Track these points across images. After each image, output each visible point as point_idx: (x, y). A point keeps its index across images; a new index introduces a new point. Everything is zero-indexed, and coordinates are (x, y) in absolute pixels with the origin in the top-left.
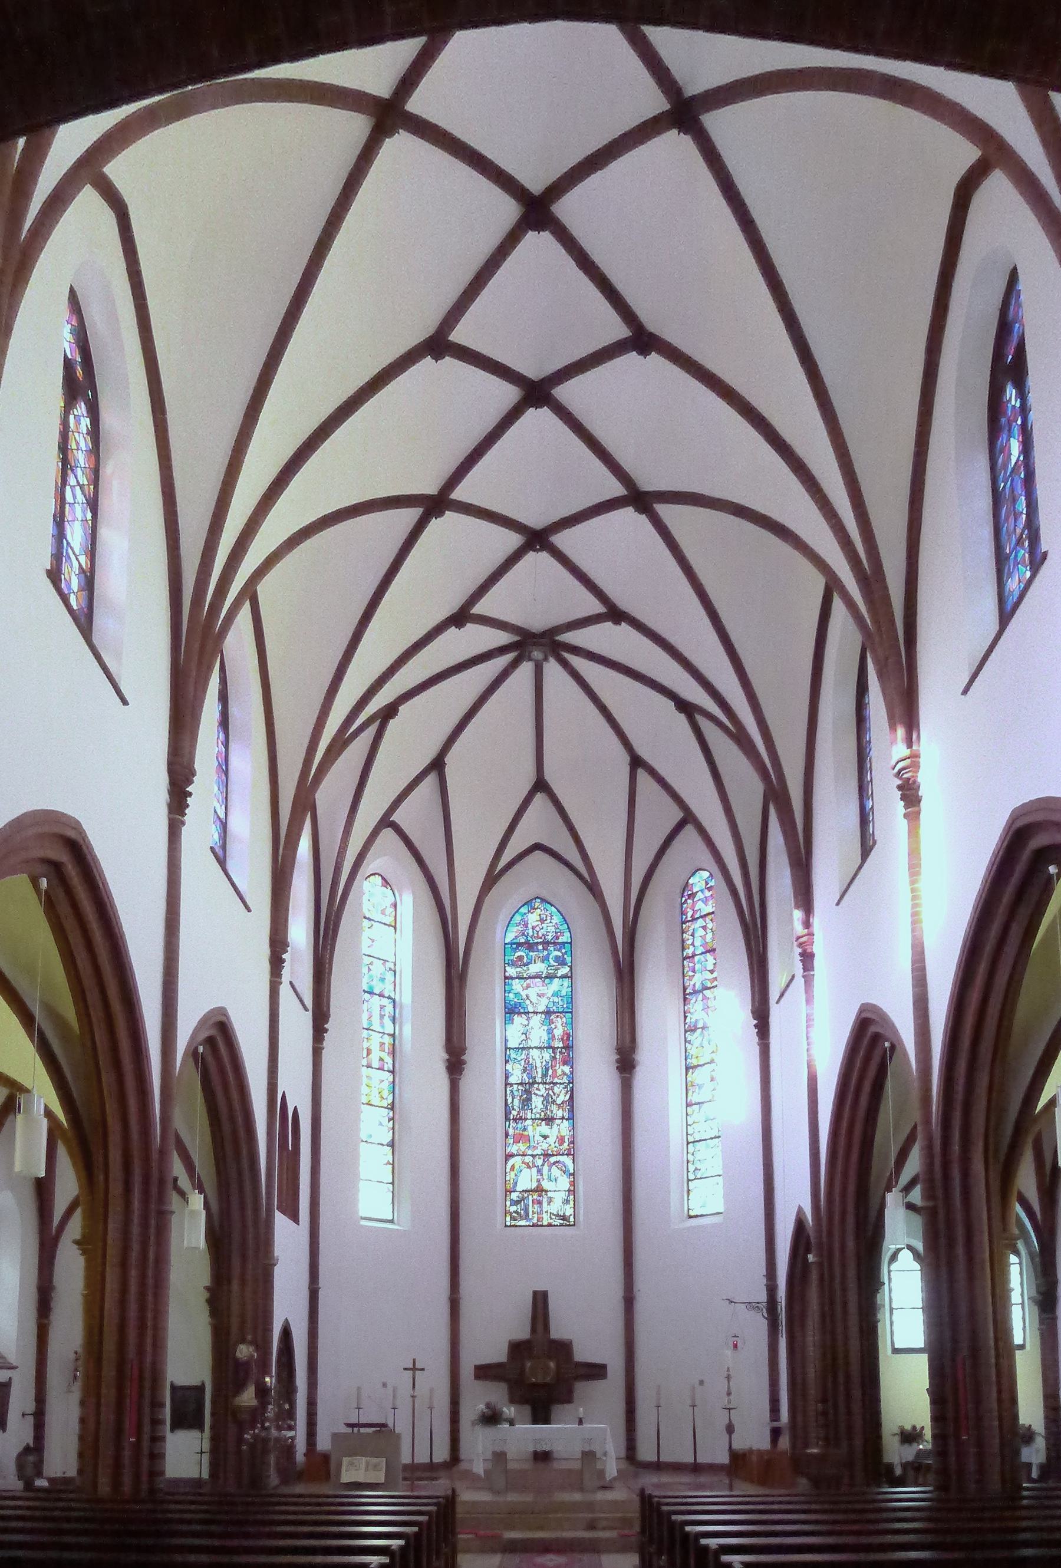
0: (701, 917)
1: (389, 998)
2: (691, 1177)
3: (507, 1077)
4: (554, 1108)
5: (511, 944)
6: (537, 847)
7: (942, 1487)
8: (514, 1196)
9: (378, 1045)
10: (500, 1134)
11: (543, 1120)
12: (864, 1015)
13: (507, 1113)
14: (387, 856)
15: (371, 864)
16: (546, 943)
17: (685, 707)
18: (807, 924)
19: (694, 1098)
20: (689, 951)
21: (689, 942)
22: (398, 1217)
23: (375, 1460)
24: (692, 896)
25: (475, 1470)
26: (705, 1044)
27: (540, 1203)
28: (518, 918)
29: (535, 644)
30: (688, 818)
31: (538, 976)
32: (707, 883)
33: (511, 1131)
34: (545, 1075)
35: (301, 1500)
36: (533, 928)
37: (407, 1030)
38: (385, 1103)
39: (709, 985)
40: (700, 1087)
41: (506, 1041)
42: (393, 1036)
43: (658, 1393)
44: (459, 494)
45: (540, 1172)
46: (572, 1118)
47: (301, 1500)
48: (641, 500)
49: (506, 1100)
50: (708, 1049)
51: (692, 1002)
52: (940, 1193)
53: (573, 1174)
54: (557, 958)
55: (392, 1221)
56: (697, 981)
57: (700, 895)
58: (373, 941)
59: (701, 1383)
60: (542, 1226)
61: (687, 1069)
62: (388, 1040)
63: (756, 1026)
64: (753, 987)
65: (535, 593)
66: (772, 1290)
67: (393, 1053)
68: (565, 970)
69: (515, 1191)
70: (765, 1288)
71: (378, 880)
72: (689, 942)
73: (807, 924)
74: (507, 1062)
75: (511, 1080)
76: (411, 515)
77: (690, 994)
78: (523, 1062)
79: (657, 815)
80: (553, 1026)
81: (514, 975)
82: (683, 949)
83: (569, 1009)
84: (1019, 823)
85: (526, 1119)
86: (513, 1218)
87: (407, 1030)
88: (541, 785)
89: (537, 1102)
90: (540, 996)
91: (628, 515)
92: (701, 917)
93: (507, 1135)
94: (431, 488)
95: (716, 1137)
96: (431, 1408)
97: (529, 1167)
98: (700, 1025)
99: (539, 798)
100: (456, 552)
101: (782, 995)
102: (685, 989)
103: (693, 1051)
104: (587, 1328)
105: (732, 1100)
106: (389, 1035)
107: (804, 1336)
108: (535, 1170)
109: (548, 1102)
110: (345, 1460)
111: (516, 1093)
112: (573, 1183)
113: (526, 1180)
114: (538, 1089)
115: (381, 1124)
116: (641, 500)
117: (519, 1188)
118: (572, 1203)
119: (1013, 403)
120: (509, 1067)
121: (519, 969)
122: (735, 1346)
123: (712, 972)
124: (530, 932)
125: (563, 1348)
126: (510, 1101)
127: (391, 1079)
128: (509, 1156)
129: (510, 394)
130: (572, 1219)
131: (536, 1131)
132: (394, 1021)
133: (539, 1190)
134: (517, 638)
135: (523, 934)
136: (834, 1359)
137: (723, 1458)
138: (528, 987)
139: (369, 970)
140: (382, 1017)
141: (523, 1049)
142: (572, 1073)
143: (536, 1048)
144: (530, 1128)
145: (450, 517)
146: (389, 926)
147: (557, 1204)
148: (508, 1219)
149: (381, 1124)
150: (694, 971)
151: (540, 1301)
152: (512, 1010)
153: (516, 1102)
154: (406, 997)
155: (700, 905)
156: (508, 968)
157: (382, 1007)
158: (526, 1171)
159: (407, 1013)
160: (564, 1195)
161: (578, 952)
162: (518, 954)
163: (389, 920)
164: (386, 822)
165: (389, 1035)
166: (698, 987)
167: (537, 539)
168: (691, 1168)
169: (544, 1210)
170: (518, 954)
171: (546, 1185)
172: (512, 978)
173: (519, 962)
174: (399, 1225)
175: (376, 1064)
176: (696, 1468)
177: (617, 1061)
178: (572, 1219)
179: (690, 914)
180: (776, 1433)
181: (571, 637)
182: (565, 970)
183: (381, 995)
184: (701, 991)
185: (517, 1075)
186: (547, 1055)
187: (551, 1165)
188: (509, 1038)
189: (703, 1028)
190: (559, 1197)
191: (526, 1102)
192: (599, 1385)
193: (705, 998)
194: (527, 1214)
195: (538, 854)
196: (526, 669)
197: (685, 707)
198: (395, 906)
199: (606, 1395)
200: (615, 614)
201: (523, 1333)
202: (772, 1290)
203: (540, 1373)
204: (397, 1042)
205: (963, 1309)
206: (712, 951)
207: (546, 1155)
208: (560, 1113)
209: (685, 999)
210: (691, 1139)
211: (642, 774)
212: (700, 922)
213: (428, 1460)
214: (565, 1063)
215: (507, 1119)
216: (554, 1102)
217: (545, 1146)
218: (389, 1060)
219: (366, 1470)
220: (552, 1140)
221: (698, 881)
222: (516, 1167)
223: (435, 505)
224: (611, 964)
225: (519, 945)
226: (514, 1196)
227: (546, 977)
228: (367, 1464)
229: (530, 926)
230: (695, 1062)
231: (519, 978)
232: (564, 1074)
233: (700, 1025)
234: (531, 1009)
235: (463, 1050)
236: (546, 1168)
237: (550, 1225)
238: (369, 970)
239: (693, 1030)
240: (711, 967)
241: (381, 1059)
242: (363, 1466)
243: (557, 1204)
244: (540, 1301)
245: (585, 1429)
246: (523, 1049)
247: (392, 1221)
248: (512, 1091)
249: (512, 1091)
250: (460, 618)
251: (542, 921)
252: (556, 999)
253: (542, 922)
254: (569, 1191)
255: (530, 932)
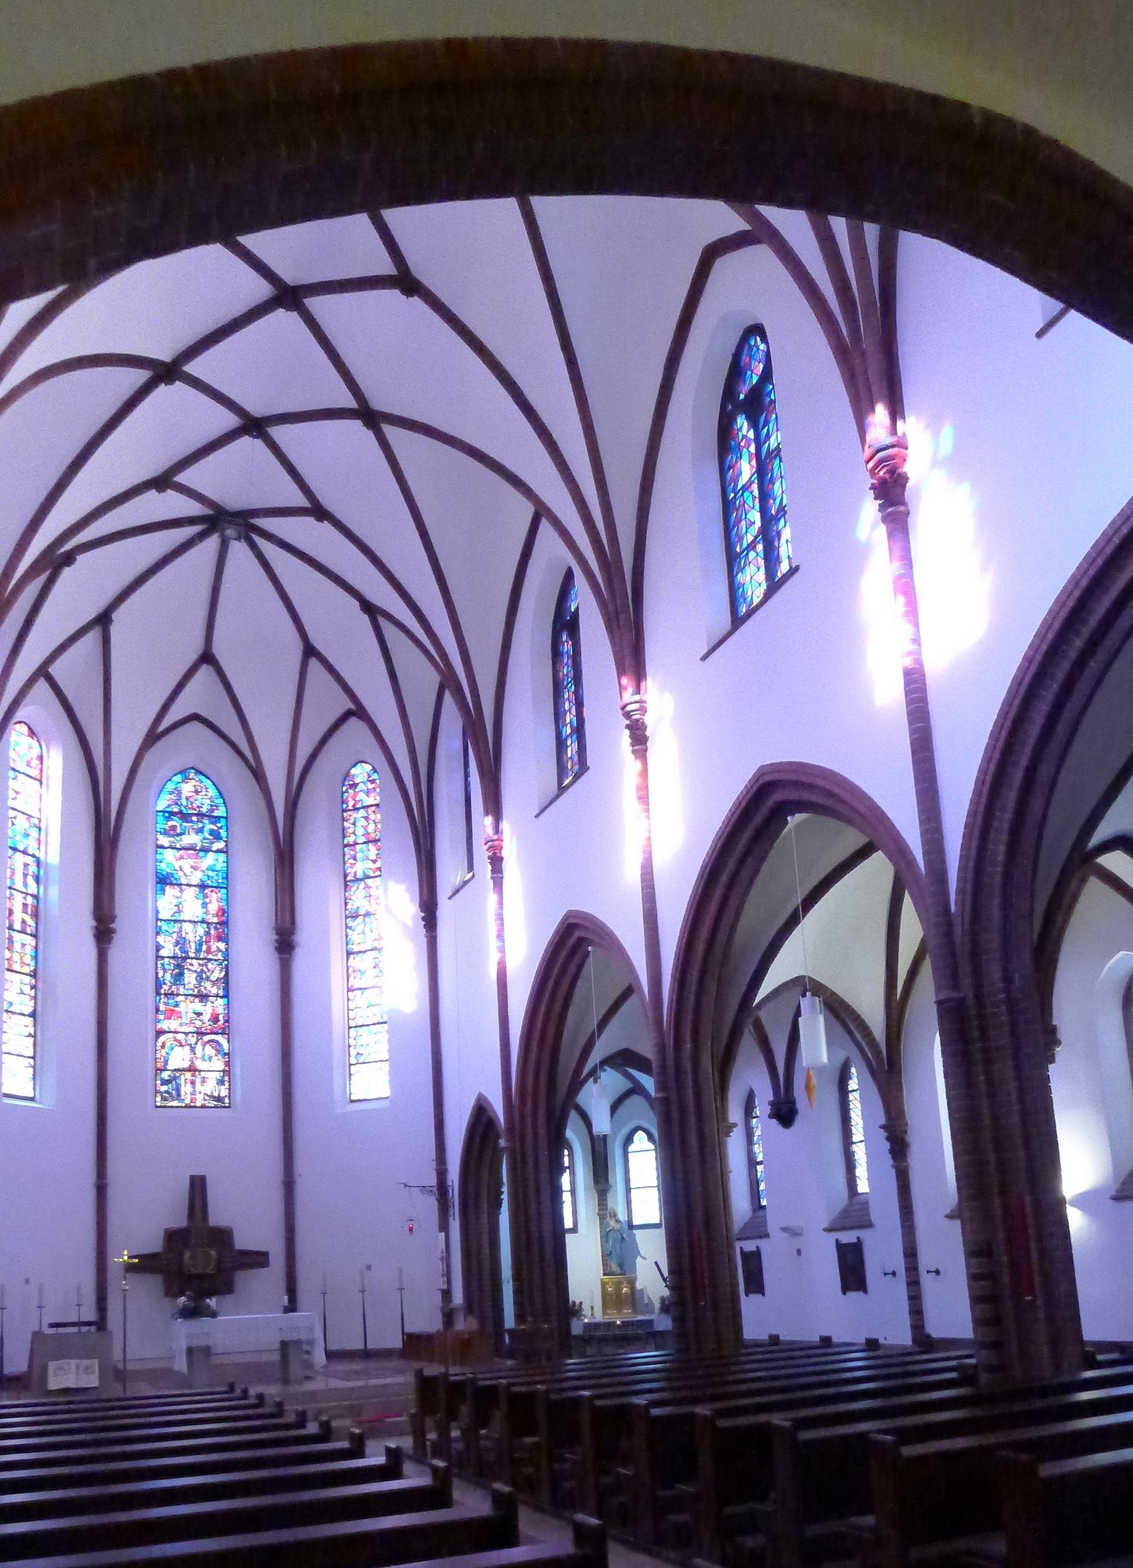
0: (363, 807)
1: (33, 856)
2: (353, 1061)
3: (158, 950)
4: (208, 985)
5: (163, 812)
6: (195, 717)
7: (683, 1349)
8: (165, 1075)
9: (21, 907)
10: (152, 1009)
11: (196, 996)
12: (571, 921)
13: (158, 984)
14: (40, 706)
15: (19, 715)
16: (200, 815)
17: (368, 608)
18: (497, 830)
19: (355, 983)
20: (350, 840)
21: (351, 830)
22: (41, 1096)
23: (86, 1362)
24: (354, 786)
25: (177, 1367)
26: (367, 930)
27: (193, 1083)
28: (170, 786)
29: (230, 523)
30: (358, 712)
31: (191, 848)
32: (369, 776)
33: (162, 1007)
34: (198, 950)
35: (110, 1404)
36: (187, 798)
37: (54, 892)
38: (27, 970)
39: (372, 874)
40: (362, 972)
41: (157, 912)
42: (36, 897)
43: (324, 1279)
44: (192, 368)
45: (193, 1050)
46: (226, 996)
47: (110, 1404)
48: (370, 417)
49: (157, 973)
50: (370, 937)
51: (354, 888)
52: (672, 1085)
53: (228, 1054)
54: (212, 832)
55: (32, 1099)
56: (359, 868)
57: (361, 787)
58: (17, 793)
59: (369, 1268)
60: (195, 1107)
61: (349, 954)
62: (30, 900)
63: (423, 919)
64: (420, 881)
65: (240, 475)
66: (442, 1173)
67: (35, 915)
68: (220, 845)
69: (166, 1070)
70: (435, 1173)
71: (24, 729)
72: (351, 830)
73: (497, 830)
74: (158, 933)
75: (162, 953)
76: (141, 376)
77: (351, 881)
78: (175, 935)
79: (324, 702)
80: (207, 900)
81: (167, 845)
82: (344, 837)
83: (227, 883)
84: (767, 778)
85: (178, 995)
86: (164, 1099)
87: (54, 892)
88: (207, 658)
89: (190, 978)
90: (195, 868)
91: (356, 426)
92: (363, 807)
93: (157, 1010)
94: (164, 353)
95: (379, 1023)
96: (363, 1291)
97: (181, 1045)
98: (362, 912)
99: (205, 671)
100: (175, 418)
101: (457, 892)
102: (346, 875)
103: (354, 936)
104: (246, 1212)
105: (399, 986)
106: (32, 895)
107: (478, 1219)
108: (188, 1048)
109: (202, 978)
110: (52, 1365)
111: (167, 967)
112: (227, 1064)
113: (178, 1058)
114: (192, 965)
115: (22, 993)
116: (370, 417)
117: (170, 1066)
118: (227, 1084)
119: (744, 431)
120: (160, 939)
121: (172, 839)
122: (411, 1229)
123: (374, 861)
124: (184, 802)
125: (222, 1237)
126: (161, 974)
127: (33, 943)
128: (159, 1033)
129: (262, 290)
130: (227, 1100)
131: (188, 1007)
132: (37, 879)
133: (192, 1069)
134: (211, 512)
135: (177, 804)
136: (528, 1238)
137: (396, 1342)
138: (182, 858)
139: (13, 824)
140: (25, 875)
141: (176, 921)
142: (227, 950)
143: (190, 921)
144: (182, 1004)
145: (369, 436)
146: (35, 779)
147: (210, 1086)
148: (158, 1099)
149: (22, 993)
150: (355, 858)
151: (198, 1186)
152: (164, 881)
153: (168, 976)
154: (53, 855)
155: (361, 796)
156: (159, 836)
157: (26, 865)
158: (177, 1049)
159: (54, 875)
160: (219, 1075)
161: (236, 829)
162: (171, 823)
163: (35, 773)
164: (43, 672)
165: (32, 895)
166: (360, 875)
167: (254, 426)
168: (353, 1052)
169: (198, 1090)
170: (171, 823)
171: (199, 1064)
172: (162, 847)
173: (170, 832)
174: (40, 1103)
175: (17, 926)
176: (366, 1354)
177: (277, 941)
178: (227, 1100)
179: (351, 803)
180: (449, 1317)
181: (264, 523)
182: (220, 845)
183: (25, 852)
184: (361, 880)
185: (168, 949)
186: (201, 930)
187: (204, 1045)
188: (160, 909)
189: (365, 915)
190: (213, 1078)
191: (179, 977)
192: (261, 1272)
193: (367, 887)
194: (179, 1095)
195: (195, 725)
196: (213, 541)
197: (368, 608)
198: (41, 758)
199: (264, 1285)
200: (319, 512)
201: (180, 1221)
202: (442, 1173)
203: (197, 1262)
204: (41, 905)
205: (697, 1189)
206: (375, 841)
207: (200, 1033)
208: (214, 990)
209: (346, 886)
210: (352, 1024)
211: (314, 663)
212: (362, 813)
213: (362, 1347)
214: (219, 939)
215: (158, 994)
216: (208, 978)
217: (198, 1023)
218: (30, 922)
219: (78, 1374)
220: (206, 1017)
221: (360, 772)
222: (168, 1045)
223: (166, 372)
224: (271, 844)
225: (172, 814)
226: (165, 1075)
227: (201, 850)
228: (78, 1367)
229: (183, 796)
230: (356, 948)
231: (171, 847)
232: (219, 950)
233: (362, 912)
234: (184, 881)
235: (112, 918)
236: (199, 1048)
237: (203, 1106)
238: (13, 824)
239: (355, 916)
240: (374, 858)
241: (24, 922)
242: (74, 1367)
243: (210, 1086)
244: (198, 1186)
245: (246, 1324)
246: (176, 921)
247: (32, 1099)
248: (163, 965)
249: (163, 965)
250: (162, 482)
251: (197, 792)
252: (211, 873)
253: (198, 793)
254: (224, 1071)
255: (184, 802)
